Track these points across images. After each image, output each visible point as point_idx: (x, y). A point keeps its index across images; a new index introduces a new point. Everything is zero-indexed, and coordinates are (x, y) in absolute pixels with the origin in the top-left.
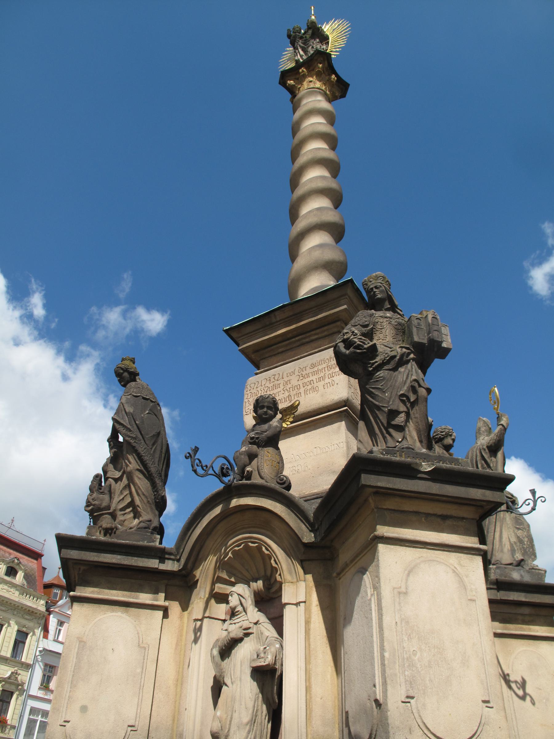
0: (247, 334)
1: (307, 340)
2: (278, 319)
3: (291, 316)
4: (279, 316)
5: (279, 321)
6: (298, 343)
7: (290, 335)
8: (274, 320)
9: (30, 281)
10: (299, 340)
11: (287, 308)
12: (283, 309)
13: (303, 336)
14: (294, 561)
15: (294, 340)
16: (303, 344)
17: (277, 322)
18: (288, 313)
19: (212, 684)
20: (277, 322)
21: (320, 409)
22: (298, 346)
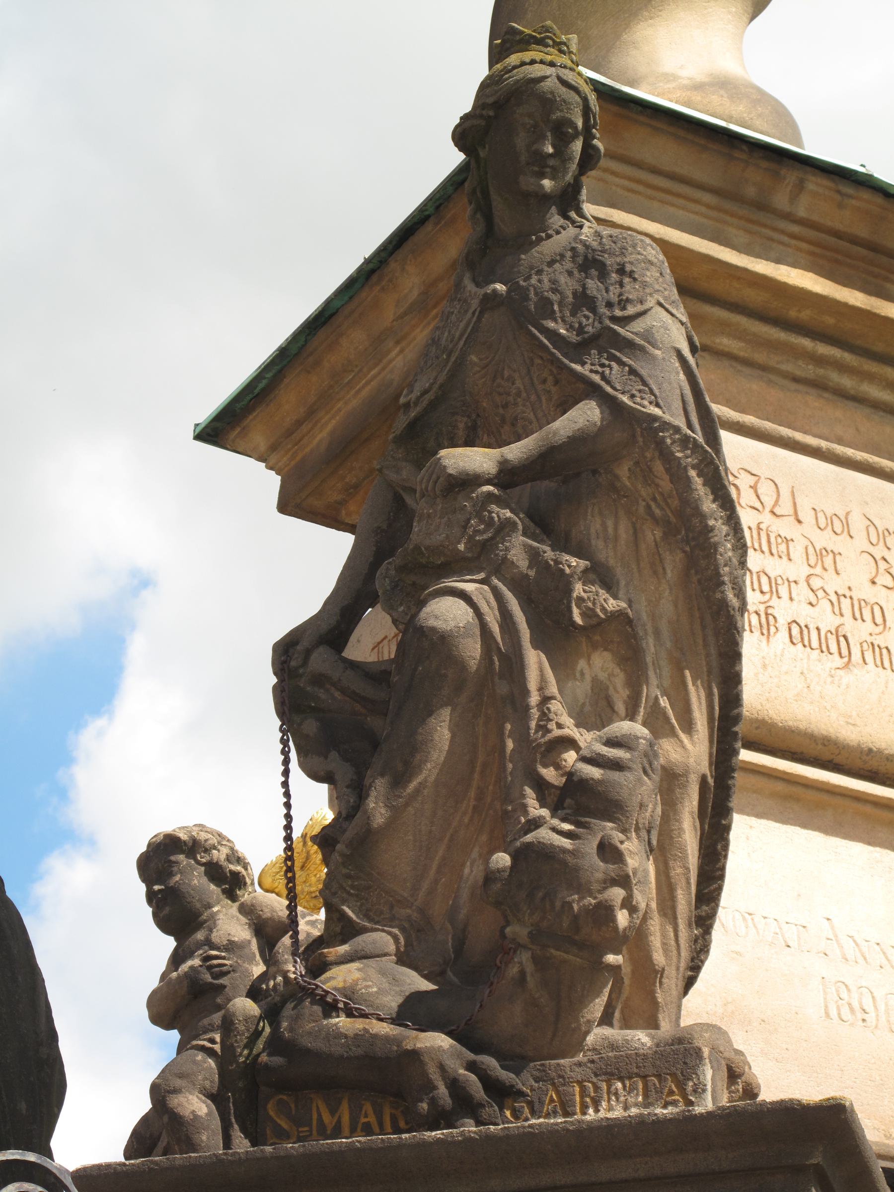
0: (638, 165)
1: (847, 382)
2: (802, 212)
3: (854, 240)
4: (814, 202)
5: (801, 222)
6: (810, 371)
7: (805, 315)
8: (781, 200)
9: (529, 845)
10: (820, 361)
11: (866, 195)
12: (849, 190)
13: (847, 357)
14: (293, 755)
15: (806, 343)
16: (819, 386)
17: (789, 217)
18: (848, 216)
19: (467, 107)
20: (789, 217)
21: (827, 741)
22: (796, 380)
